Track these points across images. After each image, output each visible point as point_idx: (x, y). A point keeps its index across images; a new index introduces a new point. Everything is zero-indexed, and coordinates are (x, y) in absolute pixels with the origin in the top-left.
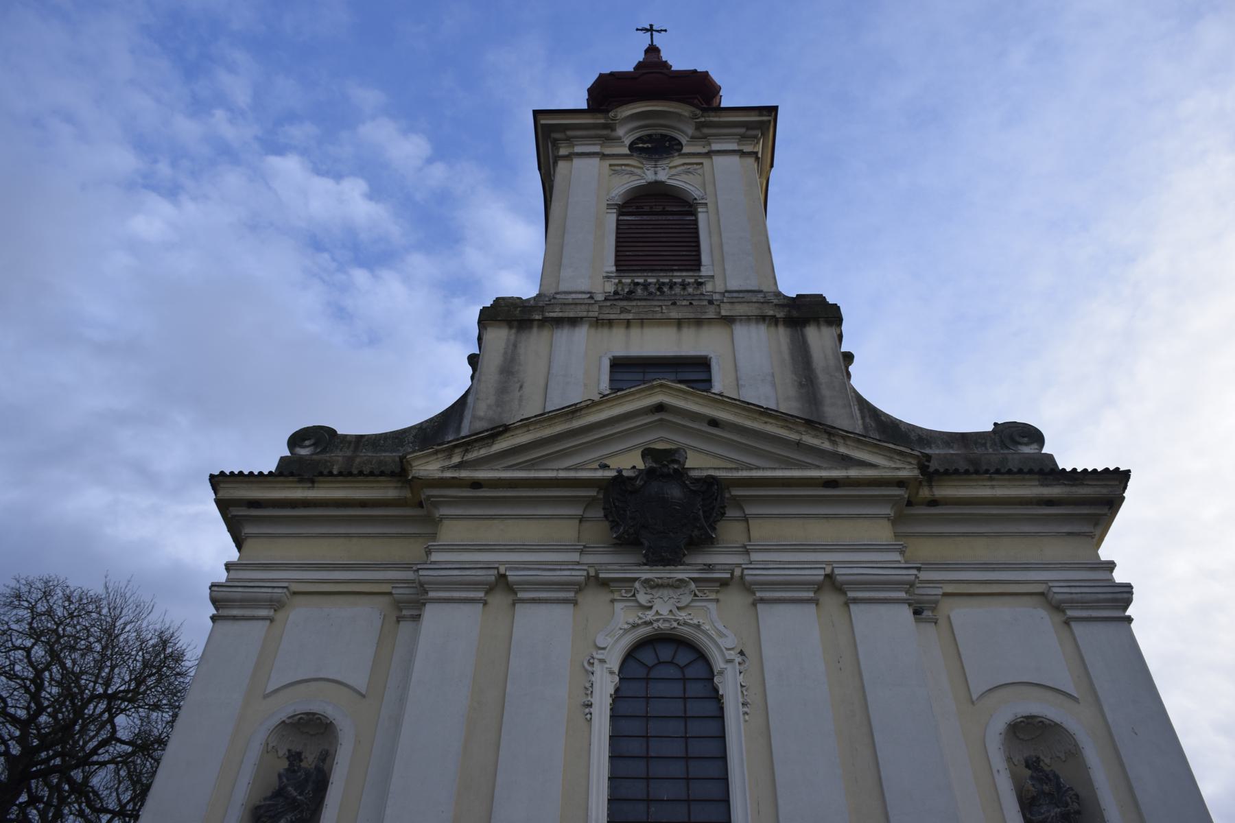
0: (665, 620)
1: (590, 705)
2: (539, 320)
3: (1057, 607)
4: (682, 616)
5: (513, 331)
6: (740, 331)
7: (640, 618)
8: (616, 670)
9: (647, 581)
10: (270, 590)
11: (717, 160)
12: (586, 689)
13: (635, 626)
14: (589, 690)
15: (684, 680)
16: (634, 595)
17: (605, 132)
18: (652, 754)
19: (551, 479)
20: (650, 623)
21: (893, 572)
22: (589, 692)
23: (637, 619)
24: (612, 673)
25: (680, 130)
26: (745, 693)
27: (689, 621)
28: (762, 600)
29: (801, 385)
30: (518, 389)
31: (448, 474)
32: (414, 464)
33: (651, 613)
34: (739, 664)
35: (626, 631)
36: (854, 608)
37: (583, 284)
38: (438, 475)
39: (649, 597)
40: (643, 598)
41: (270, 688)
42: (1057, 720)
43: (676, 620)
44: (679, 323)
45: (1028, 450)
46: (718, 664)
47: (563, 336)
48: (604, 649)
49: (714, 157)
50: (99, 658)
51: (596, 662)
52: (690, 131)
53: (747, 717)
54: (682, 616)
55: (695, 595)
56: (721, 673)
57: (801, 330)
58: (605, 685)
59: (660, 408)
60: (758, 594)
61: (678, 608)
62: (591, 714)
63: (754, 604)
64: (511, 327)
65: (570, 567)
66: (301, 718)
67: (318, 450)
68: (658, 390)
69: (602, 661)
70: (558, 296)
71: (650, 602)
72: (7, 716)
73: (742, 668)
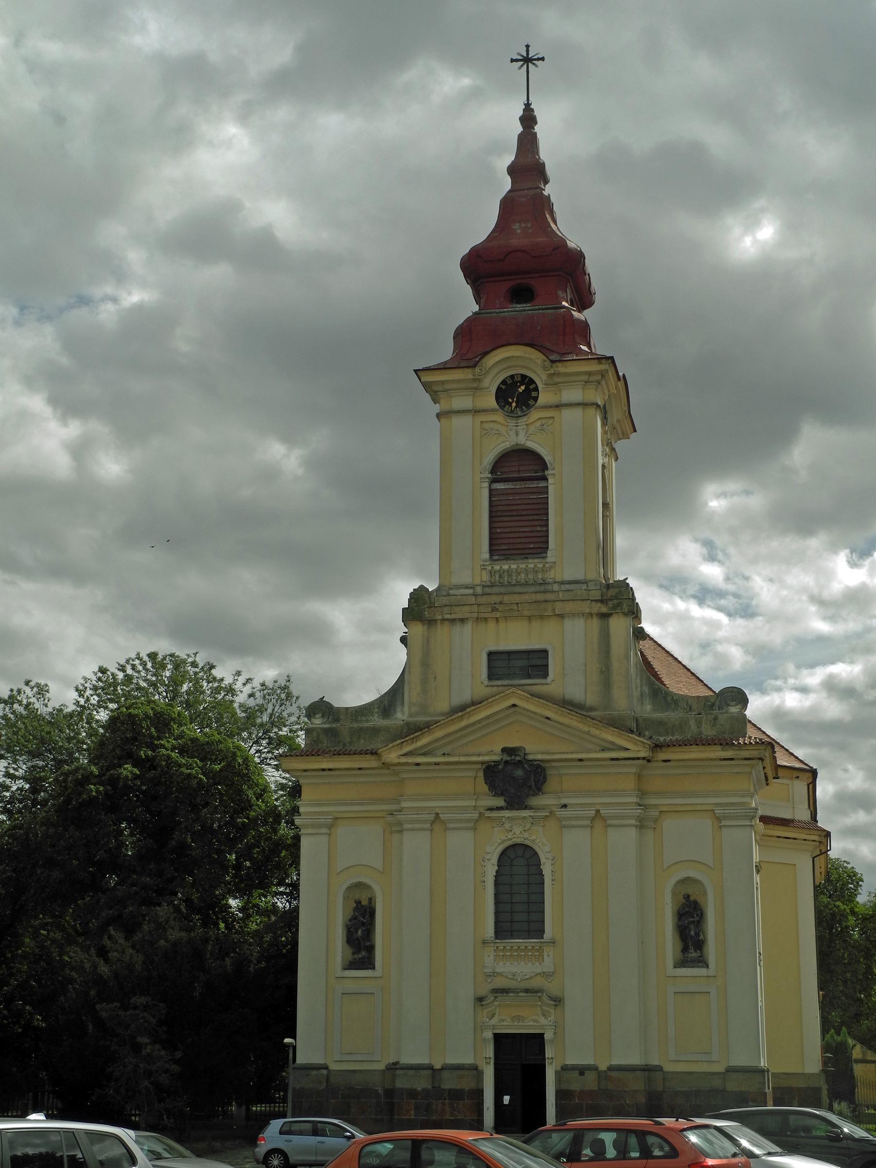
0: (518, 838)
1: (484, 882)
2: (441, 620)
3: (719, 819)
4: (526, 835)
5: (426, 627)
6: (568, 623)
7: (506, 836)
8: (496, 864)
9: (509, 817)
10: (324, 820)
11: (567, 413)
12: (483, 874)
13: (504, 841)
14: (484, 874)
15: (512, 912)
16: (503, 824)
17: (475, 385)
18: (514, 901)
19: (456, 762)
20: (511, 839)
21: (629, 811)
22: (483, 875)
23: (504, 837)
24: (493, 865)
25: (537, 374)
26: (554, 874)
27: (529, 838)
28: (564, 826)
29: (602, 672)
30: (433, 680)
31: (403, 760)
32: (383, 754)
33: (512, 833)
34: (552, 860)
35: (500, 844)
36: (609, 829)
37: (467, 579)
38: (396, 761)
39: (510, 824)
40: (507, 826)
41: (338, 872)
42: (700, 879)
43: (523, 837)
44: (530, 618)
45: (734, 710)
46: (543, 860)
47: (457, 628)
48: (490, 853)
49: (562, 411)
50: (274, 875)
51: (486, 860)
52: (544, 378)
53: (553, 886)
54: (526, 835)
55: (532, 824)
56: (544, 864)
57: (608, 620)
58: (491, 870)
59: (514, 705)
60: (563, 823)
61: (524, 827)
62: (485, 886)
63: (561, 828)
64: (424, 624)
65: (497, 377)
66: (356, 884)
67: (325, 721)
68: (512, 695)
69: (489, 860)
70: (451, 592)
71: (511, 828)
72: (518, 993)
73: (553, 862)
